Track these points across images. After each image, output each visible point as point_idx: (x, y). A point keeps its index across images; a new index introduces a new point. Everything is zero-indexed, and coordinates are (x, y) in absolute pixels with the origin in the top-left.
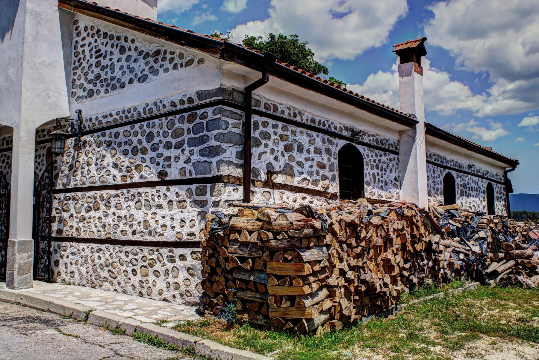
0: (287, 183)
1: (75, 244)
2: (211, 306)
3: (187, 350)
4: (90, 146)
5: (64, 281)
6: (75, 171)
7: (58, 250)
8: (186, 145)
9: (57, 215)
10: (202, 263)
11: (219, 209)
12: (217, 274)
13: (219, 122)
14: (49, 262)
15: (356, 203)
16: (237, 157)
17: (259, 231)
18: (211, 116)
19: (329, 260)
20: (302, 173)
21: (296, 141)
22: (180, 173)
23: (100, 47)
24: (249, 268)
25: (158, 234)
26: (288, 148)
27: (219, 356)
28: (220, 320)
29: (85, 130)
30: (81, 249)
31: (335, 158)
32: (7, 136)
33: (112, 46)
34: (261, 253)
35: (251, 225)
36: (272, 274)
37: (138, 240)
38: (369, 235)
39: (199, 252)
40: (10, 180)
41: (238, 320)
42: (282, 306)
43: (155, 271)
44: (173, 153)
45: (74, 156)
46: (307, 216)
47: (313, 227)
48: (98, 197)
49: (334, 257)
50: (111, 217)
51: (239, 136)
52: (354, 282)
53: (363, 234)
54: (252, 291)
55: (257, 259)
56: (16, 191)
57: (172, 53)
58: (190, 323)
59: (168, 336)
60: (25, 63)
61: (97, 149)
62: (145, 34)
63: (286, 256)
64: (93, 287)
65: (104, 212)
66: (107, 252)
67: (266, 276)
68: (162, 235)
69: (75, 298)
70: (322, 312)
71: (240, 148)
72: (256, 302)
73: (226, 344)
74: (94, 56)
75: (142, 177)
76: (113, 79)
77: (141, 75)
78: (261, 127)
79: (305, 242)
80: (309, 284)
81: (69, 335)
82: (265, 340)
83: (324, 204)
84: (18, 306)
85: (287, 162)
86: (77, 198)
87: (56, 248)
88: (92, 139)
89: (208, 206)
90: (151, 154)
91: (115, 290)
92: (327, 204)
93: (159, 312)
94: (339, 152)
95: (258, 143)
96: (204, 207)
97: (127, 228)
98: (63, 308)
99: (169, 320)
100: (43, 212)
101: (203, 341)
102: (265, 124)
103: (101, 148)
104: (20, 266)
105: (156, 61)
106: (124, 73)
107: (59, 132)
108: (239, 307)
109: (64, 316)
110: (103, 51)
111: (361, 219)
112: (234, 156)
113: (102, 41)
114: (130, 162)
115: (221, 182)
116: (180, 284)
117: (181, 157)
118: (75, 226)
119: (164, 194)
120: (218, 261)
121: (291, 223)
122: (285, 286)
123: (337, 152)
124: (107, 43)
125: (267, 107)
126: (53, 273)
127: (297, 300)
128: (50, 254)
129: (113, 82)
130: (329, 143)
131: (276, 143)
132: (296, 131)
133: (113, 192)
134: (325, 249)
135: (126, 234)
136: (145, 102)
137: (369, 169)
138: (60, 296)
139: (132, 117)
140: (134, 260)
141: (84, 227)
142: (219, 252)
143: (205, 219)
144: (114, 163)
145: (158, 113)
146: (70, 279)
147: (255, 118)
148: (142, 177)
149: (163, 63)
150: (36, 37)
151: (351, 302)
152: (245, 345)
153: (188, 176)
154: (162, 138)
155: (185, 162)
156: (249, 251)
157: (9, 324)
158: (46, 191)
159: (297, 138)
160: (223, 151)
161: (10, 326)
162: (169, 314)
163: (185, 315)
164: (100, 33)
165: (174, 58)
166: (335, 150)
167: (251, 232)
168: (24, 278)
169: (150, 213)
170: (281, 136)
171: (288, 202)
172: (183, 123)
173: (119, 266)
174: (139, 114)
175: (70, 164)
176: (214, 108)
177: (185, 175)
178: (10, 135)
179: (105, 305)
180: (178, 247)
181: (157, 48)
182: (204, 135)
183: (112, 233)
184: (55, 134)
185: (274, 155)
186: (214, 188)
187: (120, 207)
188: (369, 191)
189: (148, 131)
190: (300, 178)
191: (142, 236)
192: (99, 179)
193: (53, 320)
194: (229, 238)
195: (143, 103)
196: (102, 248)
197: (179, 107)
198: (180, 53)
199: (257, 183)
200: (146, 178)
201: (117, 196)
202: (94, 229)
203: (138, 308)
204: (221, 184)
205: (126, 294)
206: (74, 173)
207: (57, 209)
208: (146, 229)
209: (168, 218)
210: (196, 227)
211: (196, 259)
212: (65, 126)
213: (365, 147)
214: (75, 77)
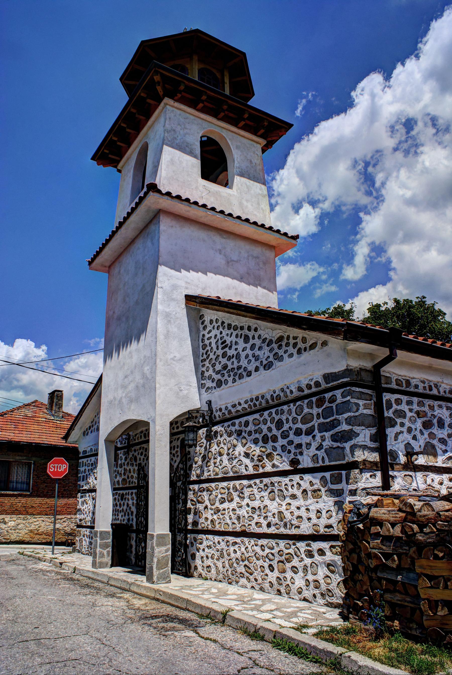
0: (431, 464)
1: (210, 537)
2: (356, 609)
3: (332, 663)
5: (200, 576)
6: (208, 461)
7: (194, 543)
8: (316, 431)
9: (192, 507)
10: (342, 559)
11: (357, 498)
12: (360, 572)
13: (349, 406)
16: (371, 440)
18: (340, 399)
20: (445, 451)
21: (435, 416)
22: (313, 460)
23: (226, 338)
24: (394, 566)
25: (293, 527)
26: (427, 425)
28: (367, 627)
29: (215, 421)
30: (216, 542)
32: (144, 429)
33: (237, 336)
34: (407, 548)
35: (393, 517)
36: (422, 573)
37: (274, 532)
39: (339, 546)
40: (148, 471)
41: (388, 627)
42: (438, 613)
43: (293, 567)
44: (304, 439)
48: (231, 488)
50: (245, 508)
51: (371, 417)
55: (403, 556)
56: (154, 484)
57: (295, 338)
58: (333, 629)
59: (310, 645)
60: (158, 361)
61: (228, 439)
62: (267, 322)
63: (436, 552)
64: (230, 583)
65: (237, 503)
66: (243, 546)
67: (415, 575)
69: (212, 596)
72: (408, 606)
73: (375, 659)
74: (220, 348)
75: (274, 466)
76: (239, 368)
77: (267, 362)
78: (394, 405)
81: (207, 639)
82: (423, 657)
84: (157, 602)
85: (428, 440)
86: (211, 489)
87: (193, 541)
89: (344, 495)
90: (281, 442)
91: (253, 587)
93: (299, 614)
95: (393, 423)
96: (340, 496)
97: (262, 520)
98: (201, 607)
99: (310, 624)
100: (179, 504)
102: (398, 402)
103: (232, 438)
104: (158, 560)
105: (280, 347)
107: (191, 424)
109: (201, 616)
110: (228, 342)
112: (368, 439)
113: (227, 332)
114: (261, 451)
115: (357, 469)
116: (320, 581)
117: (313, 444)
118: (210, 518)
119: (298, 483)
120: (359, 558)
121: (438, 513)
122: (438, 588)
124: (232, 333)
125: (398, 383)
126: (190, 567)
128: (186, 546)
129: (240, 371)
132: (434, 406)
133: (245, 482)
136: (272, 389)
138: (198, 593)
139: (260, 404)
140: (270, 555)
141: (218, 519)
142: (360, 547)
143: (342, 510)
144: (245, 453)
145: (286, 399)
146: (206, 574)
147: (386, 396)
148: (274, 466)
149: (287, 348)
150: (167, 336)
152: (399, 661)
153: (321, 463)
154: (291, 425)
155: (317, 449)
156: (393, 546)
157: (149, 622)
158: (181, 482)
159: (435, 413)
160: (355, 435)
161: (150, 625)
162: (310, 617)
163: (327, 619)
164: (225, 325)
165: (297, 342)
168: (163, 572)
169: (284, 504)
170: (418, 413)
171: (434, 485)
172: (312, 408)
174: (267, 402)
175: (202, 455)
176: (342, 390)
177: (318, 462)
178: (147, 428)
179: (242, 604)
180: (316, 541)
182: (335, 419)
183: (247, 525)
184: (187, 426)
185: (413, 433)
186: (350, 475)
187: (254, 498)
189: (277, 418)
190: (444, 457)
191: (278, 529)
192: (232, 469)
193: (191, 620)
194: (369, 532)
195: (270, 390)
196: (237, 541)
197: (306, 392)
198: (303, 337)
199: (396, 467)
200: (278, 467)
201: (250, 486)
202: (228, 521)
203: (276, 609)
204: (357, 471)
206: (207, 463)
207: (192, 500)
208: (282, 521)
209: (303, 509)
210: (333, 518)
211: (336, 554)
212: (196, 417)
214: (204, 369)
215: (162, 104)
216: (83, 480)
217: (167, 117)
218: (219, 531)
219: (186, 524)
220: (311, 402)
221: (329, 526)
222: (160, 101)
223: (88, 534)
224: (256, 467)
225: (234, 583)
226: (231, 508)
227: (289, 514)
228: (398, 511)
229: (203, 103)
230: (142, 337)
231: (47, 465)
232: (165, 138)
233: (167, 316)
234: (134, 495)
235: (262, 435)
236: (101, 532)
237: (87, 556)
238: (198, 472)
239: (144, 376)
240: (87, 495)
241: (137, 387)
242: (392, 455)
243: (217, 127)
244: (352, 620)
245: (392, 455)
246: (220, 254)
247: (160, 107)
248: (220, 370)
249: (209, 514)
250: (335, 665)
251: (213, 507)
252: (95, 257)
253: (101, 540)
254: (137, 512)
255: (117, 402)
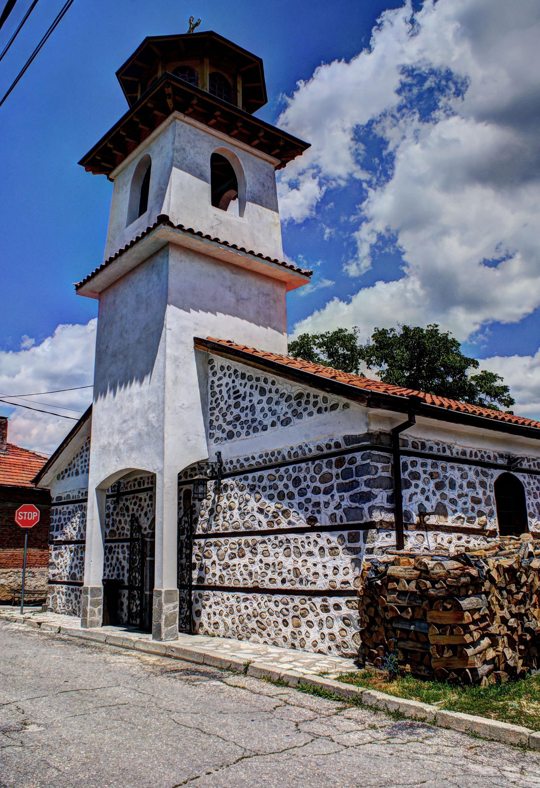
0: (441, 524)
1: (218, 593)
2: (372, 657)
4: (232, 490)
5: (206, 633)
6: (216, 515)
7: (200, 599)
8: (335, 491)
9: (197, 562)
10: (359, 612)
14: (191, 612)
15: (519, 540)
16: (388, 501)
17: (417, 580)
18: (359, 462)
19: (489, 608)
20: (455, 511)
21: (447, 478)
23: (238, 387)
24: (409, 617)
26: (439, 486)
27: (386, 705)
28: (381, 672)
29: (225, 473)
31: (491, 491)
33: (252, 387)
34: (420, 601)
37: (288, 588)
38: (530, 580)
39: (355, 601)
44: (322, 498)
45: (214, 500)
46: (465, 564)
47: (469, 575)
48: (243, 543)
49: (493, 604)
52: (517, 631)
53: (524, 579)
54: (412, 640)
55: (417, 609)
57: (316, 397)
58: (352, 675)
59: (333, 687)
60: (166, 409)
61: (240, 493)
63: (445, 604)
64: (240, 639)
68: (315, 583)
70: (485, 662)
71: (390, 492)
72: (418, 652)
73: (391, 694)
75: (290, 523)
76: (254, 421)
77: (284, 418)
78: (410, 467)
79: (463, 591)
80: (471, 633)
83: (483, 542)
85: (439, 500)
86: (220, 544)
87: (198, 597)
88: (234, 482)
89: (361, 553)
90: (298, 499)
91: (265, 642)
92: (485, 543)
93: (317, 664)
94: (495, 483)
97: (276, 576)
98: (221, 661)
101: (369, 691)
102: (414, 464)
104: (166, 617)
105: (299, 404)
106: (265, 416)
108: (401, 657)
109: (221, 669)
110: (242, 392)
111: (520, 563)
112: (385, 500)
113: (240, 382)
114: (276, 507)
117: (331, 503)
118: (218, 574)
119: (315, 541)
120: (376, 611)
121: (448, 571)
123: (493, 484)
124: (246, 384)
126: (194, 624)
127: (459, 649)
129: (255, 424)
130: (484, 476)
131: (426, 483)
133: (259, 538)
134: (483, 596)
135: (275, 582)
136: (290, 445)
137: (532, 498)
138: (211, 648)
139: (277, 459)
141: (228, 574)
142: (377, 601)
144: (259, 508)
147: (404, 459)
148: (290, 523)
149: (306, 406)
150: (175, 382)
151: (516, 651)
153: (339, 522)
154: (309, 483)
155: (335, 508)
159: (447, 475)
161: (175, 677)
166: (491, 482)
167: (409, 581)
169: (300, 560)
170: (431, 474)
171: (443, 544)
172: (331, 468)
173: (268, 616)
174: (284, 458)
176: (362, 453)
177: (336, 521)
180: (332, 596)
181: (300, 391)
183: (259, 581)
185: (426, 494)
188: (533, 523)
189: (294, 475)
190: (454, 517)
191: (293, 585)
192: (243, 524)
197: (326, 451)
198: (324, 397)
199: (410, 527)
200: (294, 524)
201: (264, 542)
204: (374, 531)
205: (277, 646)
206: (215, 517)
207: (197, 555)
208: (297, 577)
209: (320, 566)
211: (352, 608)
213: (526, 475)
214: (213, 418)
215: (171, 117)
216: (57, 530)
217: (177, 133)
218: (228, 587)
219: (191, 580)
220: (331, 462)
221: (346, 583)
222: (168, 113)
223: (65, 591)
224: (270, 523)
225: (244, 639)
226: (242, 564)
227: (305, 571)
228: (414, 569)
229: (216, 119)
230: (147, 380)
231: (14, 514)
232: (175, 159)
233: (176, 359)
234: (125, 548)
235: (278, 491)
236: (92, 589)
237: (63, 615)
238: (205, 525)
239: (148, 423)
240: (63, 547)
241: (140, 434)
242: (406, 516)
243: (228, 145)
244: (368, 667)
245: (406, 516)
246: (230, 291)
247: (168, 120)
248: (232, 421)
249: (217, 570)
250: (357, 701)
251: (222, 563)
252: (85, 282)
253: (92, 597)
254: (130, 566)
255: (112, 448)
